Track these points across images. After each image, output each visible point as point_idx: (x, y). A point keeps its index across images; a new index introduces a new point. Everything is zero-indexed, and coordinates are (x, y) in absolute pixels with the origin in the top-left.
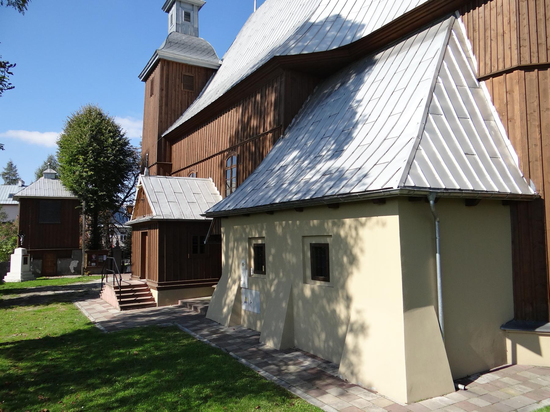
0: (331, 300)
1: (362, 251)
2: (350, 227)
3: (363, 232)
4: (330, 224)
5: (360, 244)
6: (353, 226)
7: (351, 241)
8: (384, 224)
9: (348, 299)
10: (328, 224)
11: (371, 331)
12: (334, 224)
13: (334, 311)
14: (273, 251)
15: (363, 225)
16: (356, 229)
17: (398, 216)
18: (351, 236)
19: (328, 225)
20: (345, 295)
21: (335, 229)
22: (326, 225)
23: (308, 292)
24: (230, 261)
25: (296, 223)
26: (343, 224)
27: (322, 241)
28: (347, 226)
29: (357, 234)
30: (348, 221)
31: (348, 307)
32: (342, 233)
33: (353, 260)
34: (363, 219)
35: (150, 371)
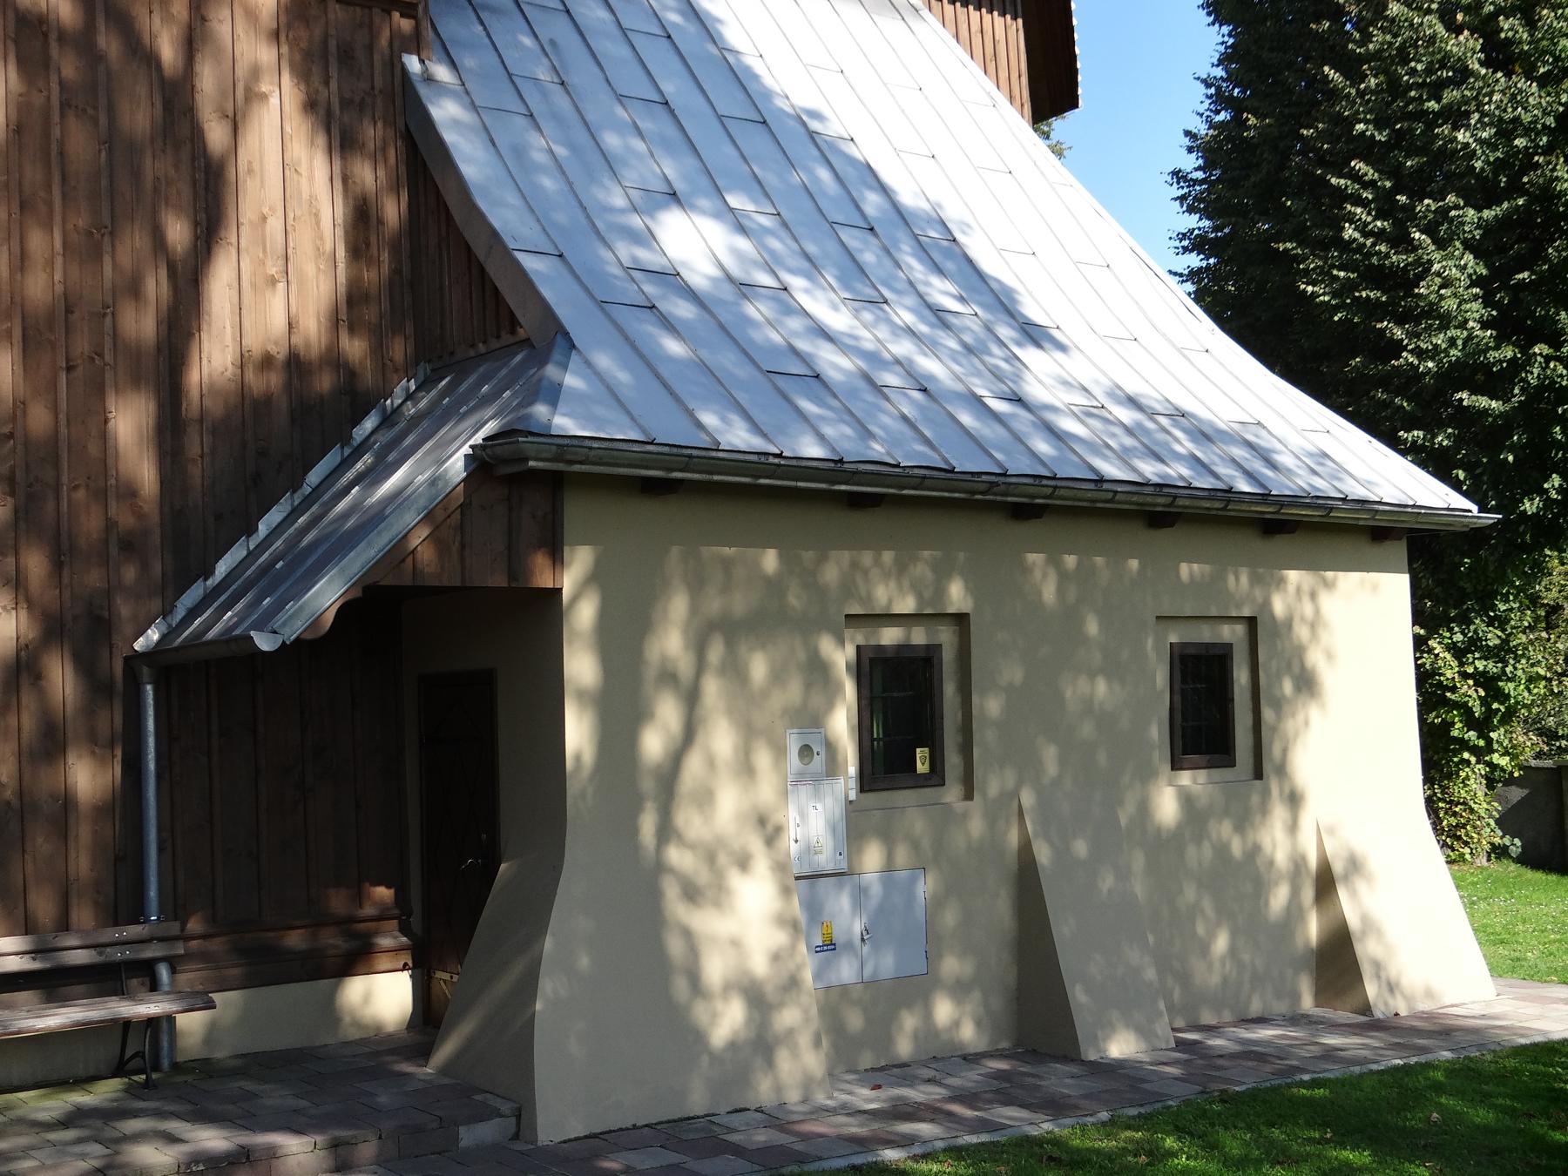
0: (1245, 820)
1: (1330, 656)
2: (1299, 590)
3: (1329, 603)
4: (1244, 580)
5: (1324, 636)
6: (1306, 588)
7: (1302, 632)
8: (1375, 588)
9: (1294, 800)
10: (1237, 579)
11: (1374, 862)
12: (1255, 580)
13: (1254, 851)
14: (1013, 673)
15: (1329, 585)
16: (1313, 596)
17: (406, 975)
18: (1303, 619)
19: (1240, 581)
20: (1287, 791)
21: (1258, 594)
22: (1231, 579)
23: (1166, 805)
24: (653, 744)
25: (1128, 562)
26: (1282, 581)
27: (1205, 634)
28: (1291, 588)
29: (1317, 611)
30: (1293, 576)
31: (1293, 827)
32: (1279, 606)
33: (1307, 683)
34: (1329, 574)
35: (371, 607)
